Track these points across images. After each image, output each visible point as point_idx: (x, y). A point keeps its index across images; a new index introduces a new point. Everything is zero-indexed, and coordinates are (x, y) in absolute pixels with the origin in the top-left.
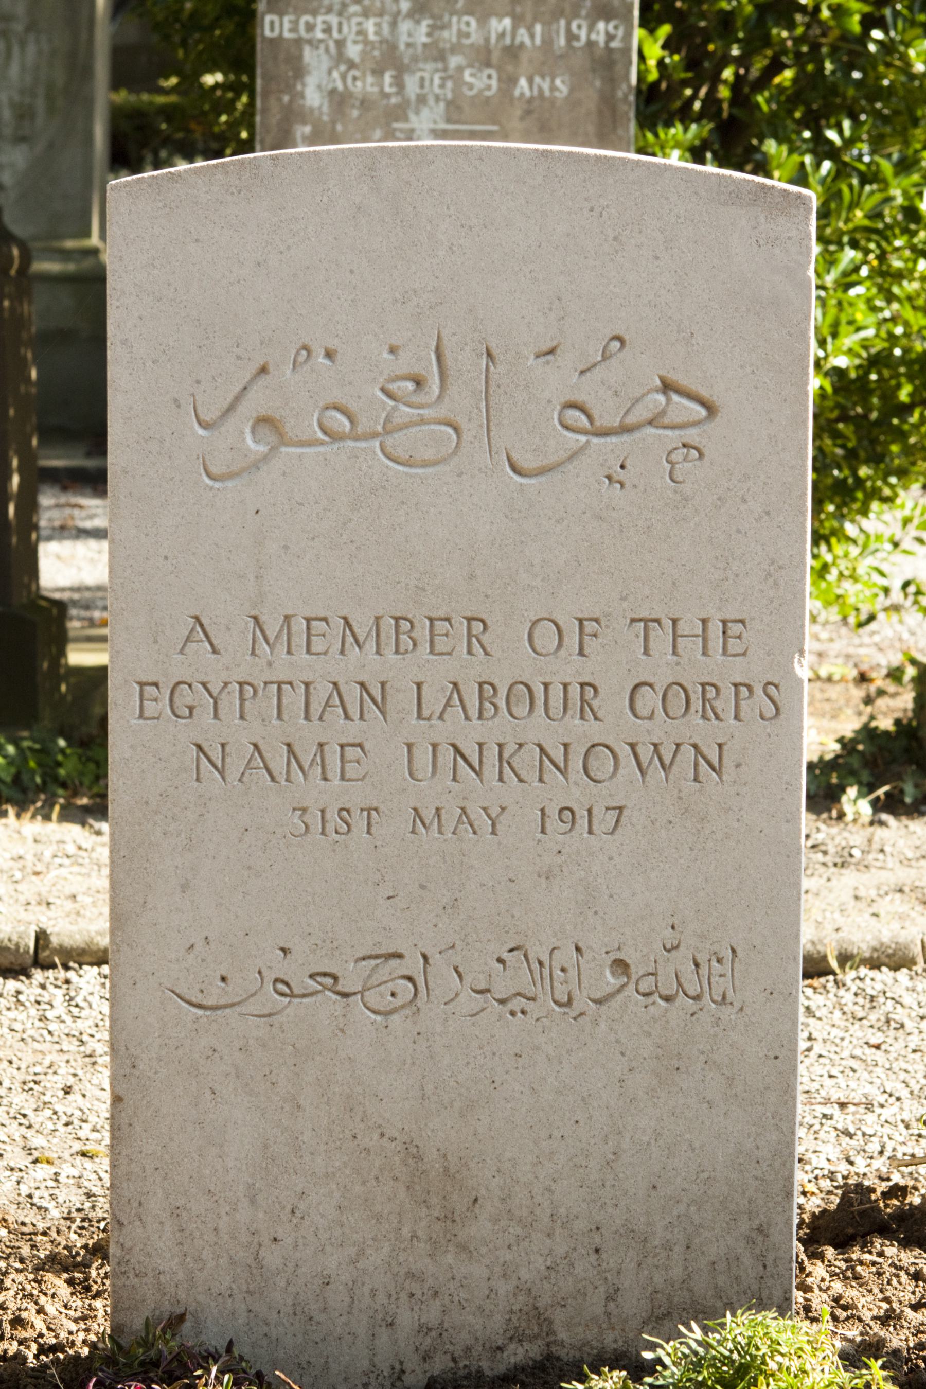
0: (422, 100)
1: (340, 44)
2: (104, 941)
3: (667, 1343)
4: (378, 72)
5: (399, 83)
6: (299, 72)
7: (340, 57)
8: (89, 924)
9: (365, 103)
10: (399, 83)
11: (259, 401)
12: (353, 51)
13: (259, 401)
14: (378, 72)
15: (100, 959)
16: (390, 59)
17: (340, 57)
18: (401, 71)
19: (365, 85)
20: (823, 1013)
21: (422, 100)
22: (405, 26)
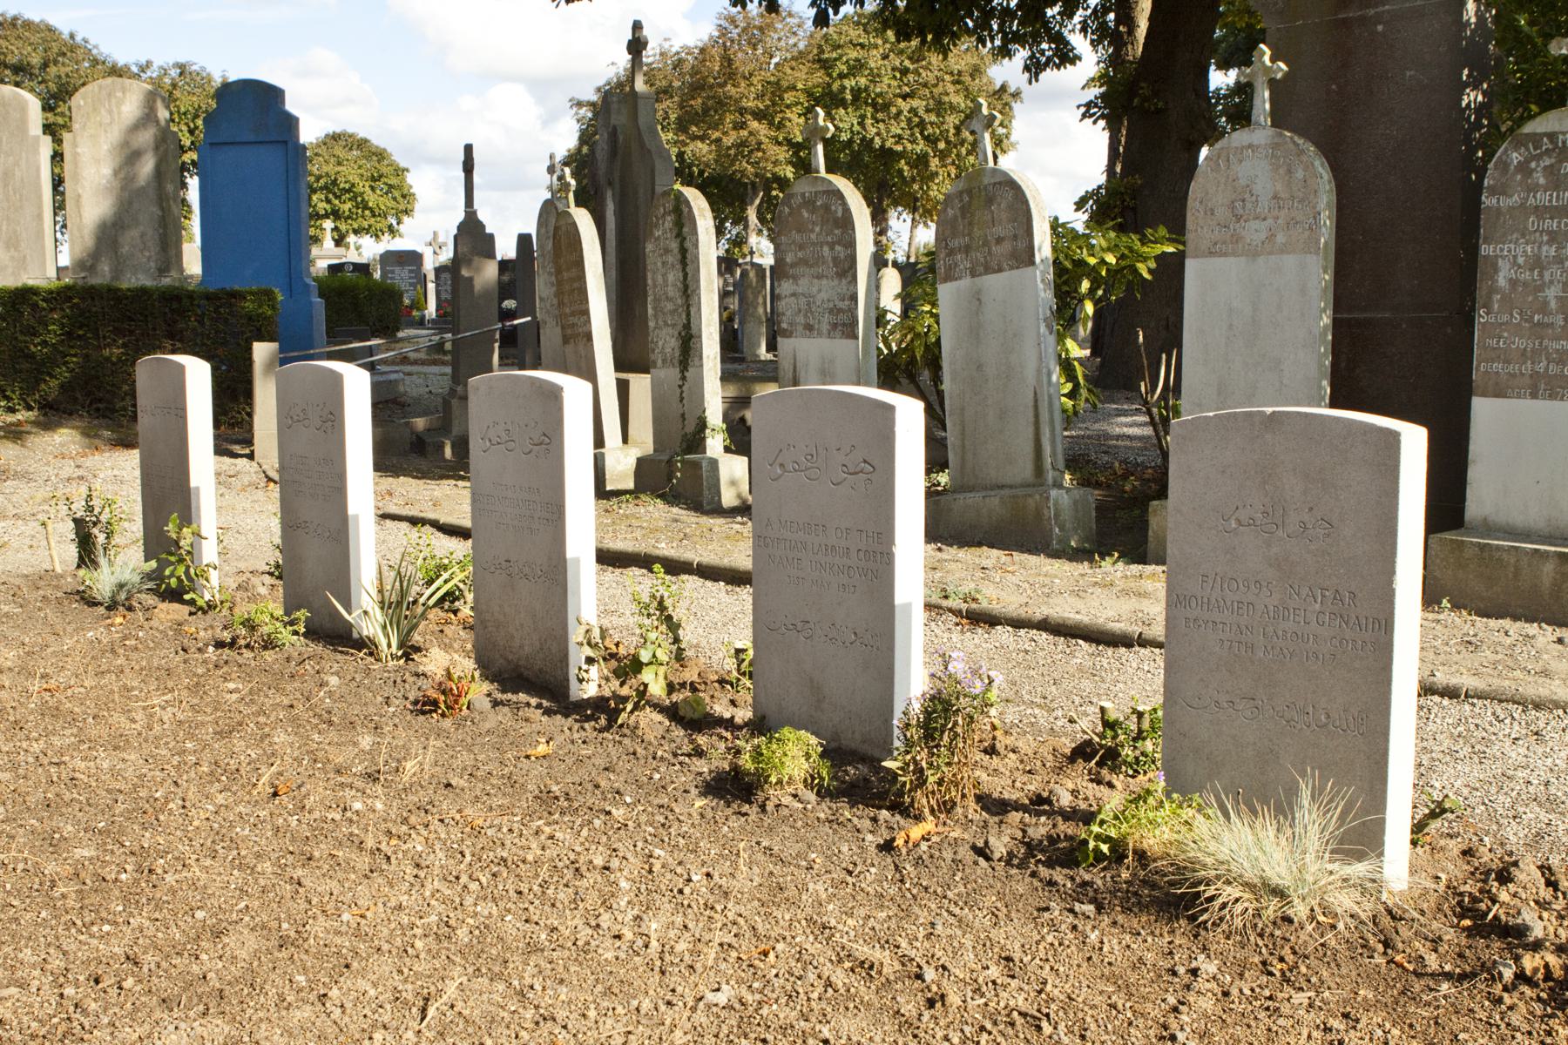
0: (1551, 282)
1: (1515, 257)
2: (1162, 639)
3: (453, 341)
4: (1532, 270)
5: (1541, 275)
6: (1496, 270)
7: (1515, 263)
8: (1158, 631)
9: (1525, 284)
10: (1541, 275)
11: (779, 460)
12: (1521, 260)
13: (779, 460)
14: (1532, 270)
15: (1160, 645)
16: (1537, 263)
17: (1515, 263)
18: (1542, 269)
19: (1526, 276)
20: (1158, 631)
21: (1551, 282)
22: (1545, 248)
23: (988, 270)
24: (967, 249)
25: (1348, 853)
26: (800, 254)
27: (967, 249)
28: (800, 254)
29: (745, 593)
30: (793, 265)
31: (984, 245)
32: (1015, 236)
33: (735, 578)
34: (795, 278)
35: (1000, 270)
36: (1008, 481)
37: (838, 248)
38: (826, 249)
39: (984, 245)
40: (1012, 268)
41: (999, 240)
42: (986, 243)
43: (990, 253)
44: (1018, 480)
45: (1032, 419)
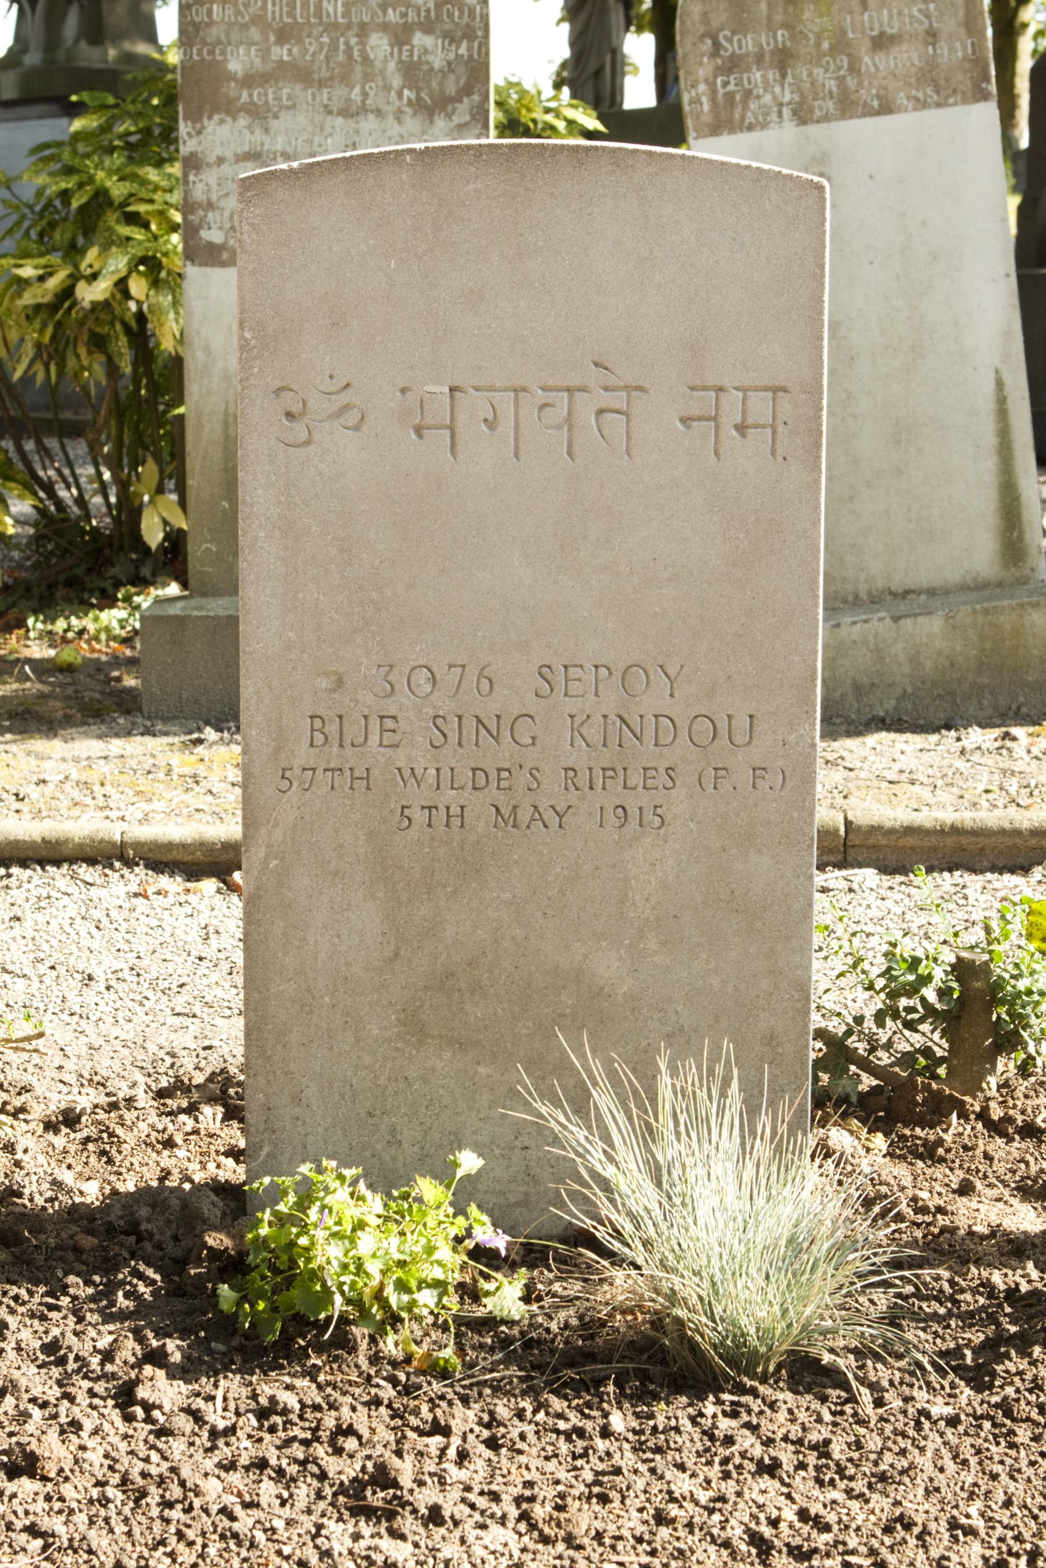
23: (848, 106)
24: (783, 60)
25: (715, 1378)
26: (281, 53)
27: (783, 60)
28: (281, 53)
29: (827, 814)
30: (248, 81)
31: (834, 51)
32: (932, 36)
33: (210, 863)
34: (260, 115)
35: (886, 109)
36: (923, 578)
37: (421, 40)
38: (379, 45)
39: (834, 51)
40: (922, 105)
41: (881, 42)
42: (841, 45)
43: (854, 68)
44: (953, 576)
45: (990, 439)
